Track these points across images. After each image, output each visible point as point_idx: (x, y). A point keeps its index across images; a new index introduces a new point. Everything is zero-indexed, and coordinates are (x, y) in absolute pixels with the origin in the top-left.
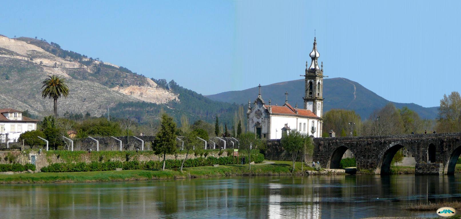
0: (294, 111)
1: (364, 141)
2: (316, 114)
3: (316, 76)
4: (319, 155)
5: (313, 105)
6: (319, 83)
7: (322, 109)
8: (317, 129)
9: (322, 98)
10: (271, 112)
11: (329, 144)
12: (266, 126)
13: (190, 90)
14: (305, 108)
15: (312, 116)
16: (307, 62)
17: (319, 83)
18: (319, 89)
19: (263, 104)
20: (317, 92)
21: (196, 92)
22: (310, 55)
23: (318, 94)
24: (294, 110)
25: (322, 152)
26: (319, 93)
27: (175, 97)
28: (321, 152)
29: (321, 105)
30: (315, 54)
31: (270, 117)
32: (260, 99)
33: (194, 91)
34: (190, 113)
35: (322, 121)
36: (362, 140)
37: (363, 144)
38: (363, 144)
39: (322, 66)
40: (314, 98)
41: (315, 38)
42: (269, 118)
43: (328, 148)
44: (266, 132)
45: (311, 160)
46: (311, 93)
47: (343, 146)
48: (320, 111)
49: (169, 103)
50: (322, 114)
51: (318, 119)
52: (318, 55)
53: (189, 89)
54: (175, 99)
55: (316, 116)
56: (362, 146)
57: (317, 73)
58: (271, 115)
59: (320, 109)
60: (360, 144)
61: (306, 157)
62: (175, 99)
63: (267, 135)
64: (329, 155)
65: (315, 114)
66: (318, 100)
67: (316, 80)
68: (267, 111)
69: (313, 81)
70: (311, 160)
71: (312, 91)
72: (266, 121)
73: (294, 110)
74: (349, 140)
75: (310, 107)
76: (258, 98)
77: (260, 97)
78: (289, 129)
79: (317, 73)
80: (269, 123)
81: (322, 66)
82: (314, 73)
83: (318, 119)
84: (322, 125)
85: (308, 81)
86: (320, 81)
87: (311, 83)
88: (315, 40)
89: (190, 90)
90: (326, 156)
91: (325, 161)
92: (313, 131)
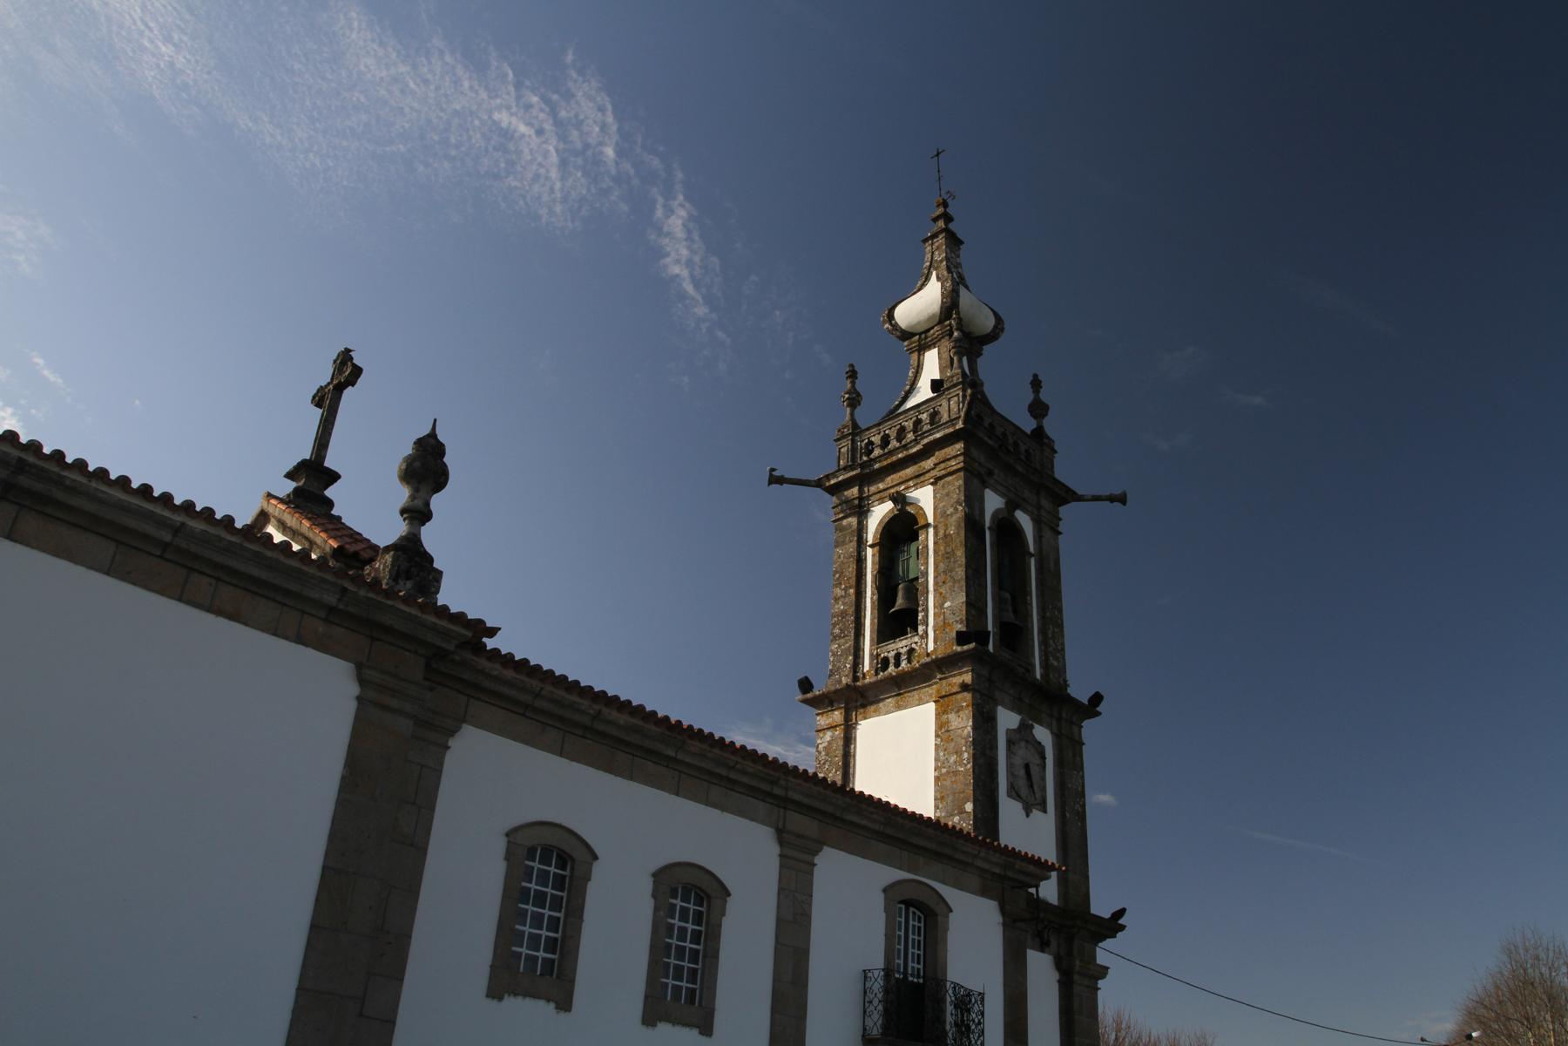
16: (853, 374)
26: (1010, 617)
39: (1038, 409)
81: (1038, 409)
85: (880, 512)
86: (924, 498)
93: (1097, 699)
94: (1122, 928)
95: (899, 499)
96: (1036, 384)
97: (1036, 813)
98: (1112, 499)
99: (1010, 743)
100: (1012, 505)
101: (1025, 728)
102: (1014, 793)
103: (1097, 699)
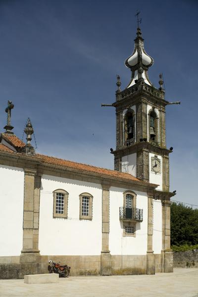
6: (153, 114)
8: (150, 215)
17: (153, 114)
22: (127, 63)
26: (152, 133)
39: (161, 83)
50: (168, 222)
52: (146, 58)
69: (134, 108)
86: (157, 111)
87: (129, 117)
93: (171, 149)
94: (175, 194)
95: (156, 157)
98: (104, 106)
99: (152, 160)
100: (154, 108)
101: (156, 157)
102: (153, 170)
103: (171, 149)
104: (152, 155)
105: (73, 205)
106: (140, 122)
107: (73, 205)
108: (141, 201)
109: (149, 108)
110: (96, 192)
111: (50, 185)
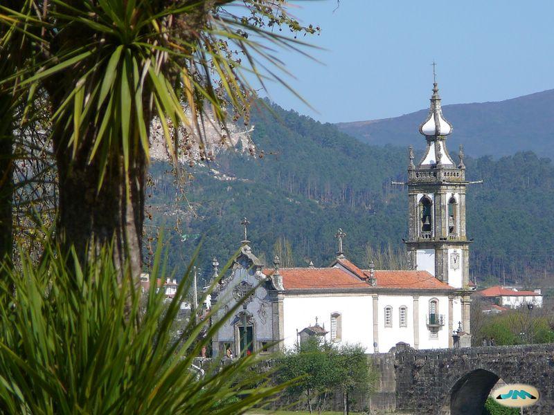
0: (365, 279)
1: (541, 356)
2: (447, 280)
3: (441, 184)
4: (412, 392)
5: (436, 256)
6: (452, 201)
7: (467, 265)
8: (451, 318)
9: (464, 239)
10: (280, 286)
11: (442, 366)
12: (269, 322)
13: (292, 110)
14: (413, 266)
15: (437, 288)
17: (452, 201)
18: (452, 215)
19: (255, 268)
20: (447, 223)
21: (311, 119)
22: (421, 130)
23: (451, 229)
24: (364, 277)
25: (422, 385)
26: (452, 225)
27: (240, 137)
28: (419, 385)
29: (463, 256)
30: (435, 126)
31: (277, 299)
32: (246, 257)
33: (303, 116)
34: (287, 195)
35: (468, 298)
36: (533, 353)
37: (538, 363)
38: (538, 363)
40: (438, 239)
41: (435, 85)
42: (275, 301)
43: (440, 376)
44: (268, 337)
45: (391, 406)
46: (427, 228)
47: (480, 369)
48: (459, 272)
49: (218, 156)
51: (452, 293)
53: (289, 110)
54: (239, 145)
55: (447, 288)
56: (534, 369)
57: (443, 174)
58: (280, 296)
59: (461, 267)
60: (530, 365)
61: (373, 400)
62: (239, 145)
63: (271, 344)
64: (442, 391)
65: (441, 281)
66: (449, 244)
67: (440, 194)
68: (268, 284)
69: (430, 196)
70: (391, 406)
71: (430, 221)
72: (268, 310)
73: (364, 274)
74: (499, 355)
75: (425, 261)
76: (242, 255)
77: (245, 250)
78: (320, 331)
79: (443, 174)
80: (276, 314)
82: (435, 175)
83: (452, 293)
84: (468, 307)
86: (457, 196)
87: (426, 202)
88: (435, 91)
89: (292, 110)
90: (434, 395)
91: (431, 407)
92: (434, 326)
96: (317, 319)
97: (457, 270)
102: (452, 267)
104: (451, 250)
105: (396, 314)
106: (439, 215)
107: (396, 314)
108: (443, 301)
109: (448, 196)
110: (407, 300)
111: (384, 300)
